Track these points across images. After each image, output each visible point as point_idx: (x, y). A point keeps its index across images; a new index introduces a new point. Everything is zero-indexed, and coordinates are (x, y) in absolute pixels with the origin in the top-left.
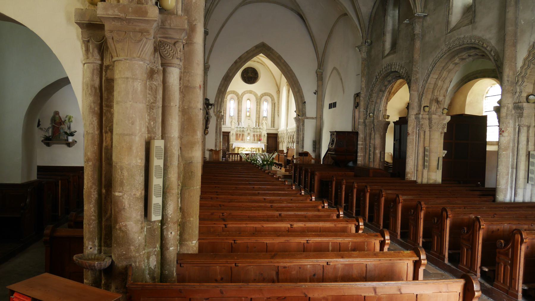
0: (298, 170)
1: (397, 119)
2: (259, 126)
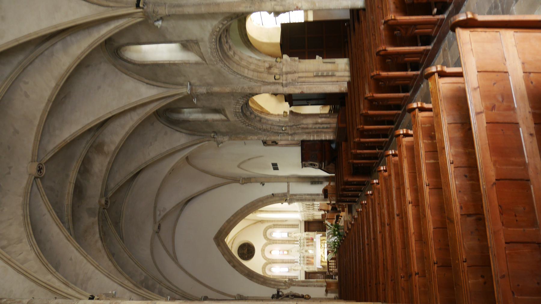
0: (342, 198)
1: (287, 103)
2: (297, 241)
